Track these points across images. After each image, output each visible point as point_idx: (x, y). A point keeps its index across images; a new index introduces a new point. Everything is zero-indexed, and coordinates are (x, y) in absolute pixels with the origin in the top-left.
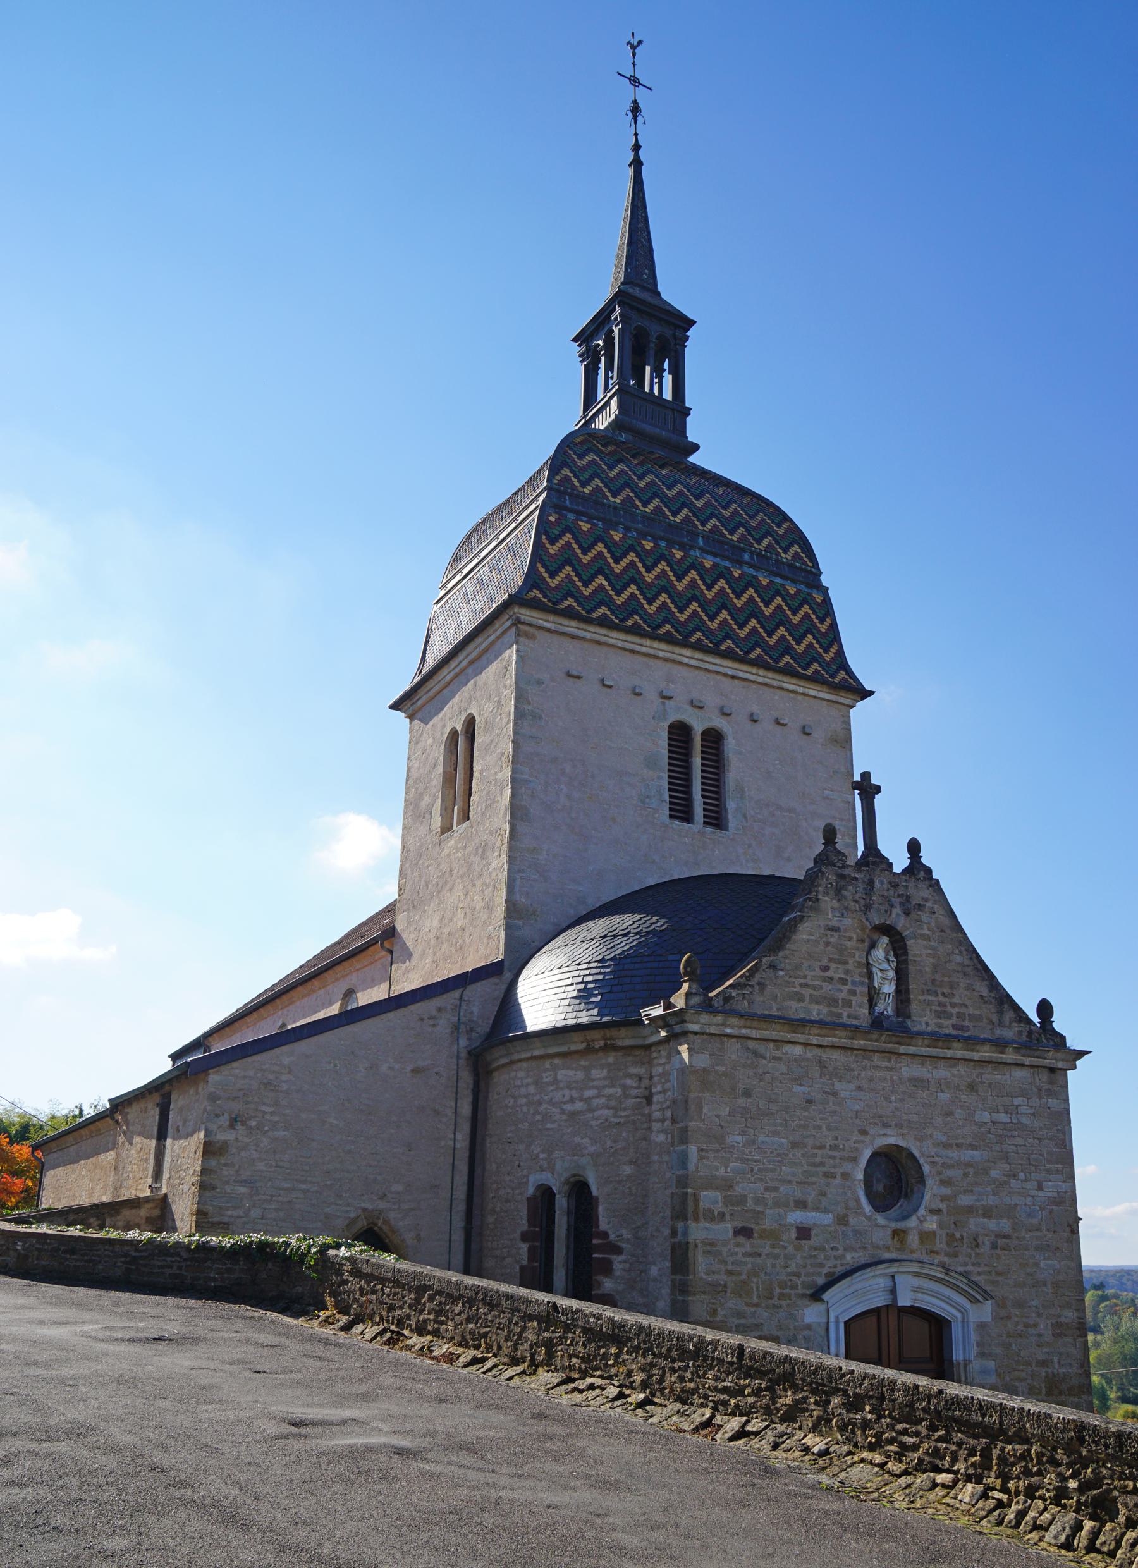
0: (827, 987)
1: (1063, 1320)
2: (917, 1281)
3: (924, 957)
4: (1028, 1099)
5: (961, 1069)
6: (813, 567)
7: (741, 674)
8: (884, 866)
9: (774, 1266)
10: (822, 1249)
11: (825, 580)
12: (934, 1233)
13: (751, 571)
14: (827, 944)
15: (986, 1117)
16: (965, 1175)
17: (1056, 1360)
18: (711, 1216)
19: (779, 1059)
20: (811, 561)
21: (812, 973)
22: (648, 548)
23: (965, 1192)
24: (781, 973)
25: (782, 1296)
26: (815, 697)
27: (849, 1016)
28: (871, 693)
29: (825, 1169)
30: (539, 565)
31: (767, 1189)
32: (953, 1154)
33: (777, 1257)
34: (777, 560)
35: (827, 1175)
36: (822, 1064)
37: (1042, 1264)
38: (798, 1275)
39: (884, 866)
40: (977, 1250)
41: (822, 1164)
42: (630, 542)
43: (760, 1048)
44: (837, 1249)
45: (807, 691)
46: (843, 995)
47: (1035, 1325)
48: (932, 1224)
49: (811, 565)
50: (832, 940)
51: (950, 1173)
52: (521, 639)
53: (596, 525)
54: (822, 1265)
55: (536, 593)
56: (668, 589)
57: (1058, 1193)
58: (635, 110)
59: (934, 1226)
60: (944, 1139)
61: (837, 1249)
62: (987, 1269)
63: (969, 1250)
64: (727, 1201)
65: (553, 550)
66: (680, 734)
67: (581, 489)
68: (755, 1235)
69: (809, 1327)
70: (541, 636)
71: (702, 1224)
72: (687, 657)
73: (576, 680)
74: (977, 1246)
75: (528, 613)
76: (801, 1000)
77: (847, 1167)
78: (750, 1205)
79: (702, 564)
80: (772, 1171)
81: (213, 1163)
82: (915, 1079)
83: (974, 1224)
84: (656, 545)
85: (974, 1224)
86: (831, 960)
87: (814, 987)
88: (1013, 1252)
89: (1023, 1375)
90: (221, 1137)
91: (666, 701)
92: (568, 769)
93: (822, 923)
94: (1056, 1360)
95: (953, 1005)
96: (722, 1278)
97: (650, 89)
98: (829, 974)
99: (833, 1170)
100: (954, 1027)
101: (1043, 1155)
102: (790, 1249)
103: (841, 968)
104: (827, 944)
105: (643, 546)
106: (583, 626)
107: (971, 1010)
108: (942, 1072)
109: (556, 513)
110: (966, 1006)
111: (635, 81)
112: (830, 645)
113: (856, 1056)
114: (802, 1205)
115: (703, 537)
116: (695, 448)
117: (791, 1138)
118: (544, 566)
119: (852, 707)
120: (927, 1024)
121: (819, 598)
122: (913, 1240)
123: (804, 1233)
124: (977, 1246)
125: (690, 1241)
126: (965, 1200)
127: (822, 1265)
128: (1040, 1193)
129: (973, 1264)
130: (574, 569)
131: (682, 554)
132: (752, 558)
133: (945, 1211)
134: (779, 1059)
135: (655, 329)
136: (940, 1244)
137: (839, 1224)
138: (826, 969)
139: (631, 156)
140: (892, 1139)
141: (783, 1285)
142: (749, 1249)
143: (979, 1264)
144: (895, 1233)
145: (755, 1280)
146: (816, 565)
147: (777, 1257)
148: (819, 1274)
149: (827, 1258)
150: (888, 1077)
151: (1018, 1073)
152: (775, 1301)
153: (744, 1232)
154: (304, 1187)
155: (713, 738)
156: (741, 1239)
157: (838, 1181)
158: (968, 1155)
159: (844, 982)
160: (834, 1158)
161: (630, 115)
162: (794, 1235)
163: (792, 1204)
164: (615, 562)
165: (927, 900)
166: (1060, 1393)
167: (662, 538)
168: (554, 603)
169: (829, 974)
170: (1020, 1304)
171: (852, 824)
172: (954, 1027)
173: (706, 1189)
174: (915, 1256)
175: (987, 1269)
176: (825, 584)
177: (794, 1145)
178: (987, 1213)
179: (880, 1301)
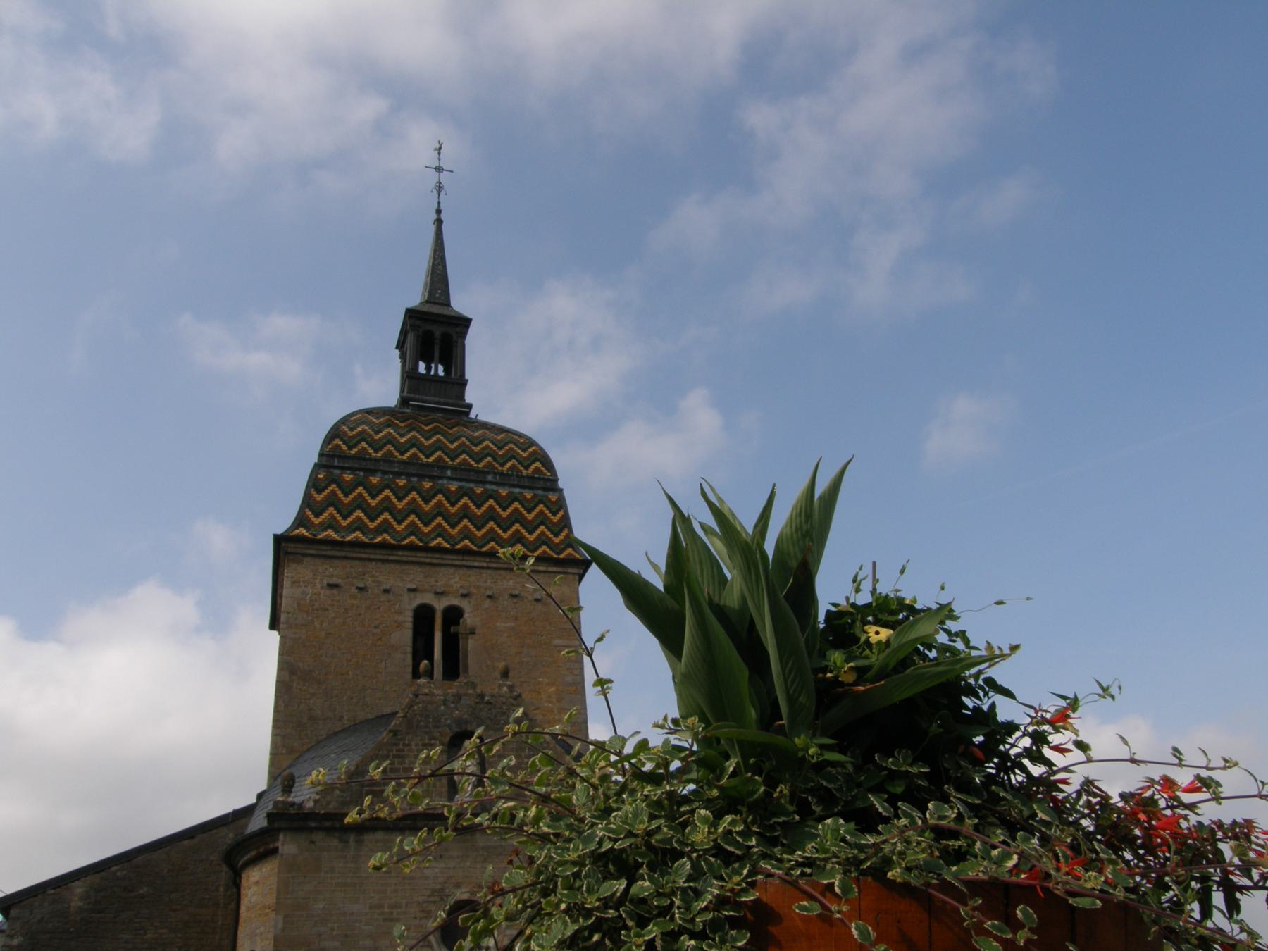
6: (551, 476)
7: (476, 564)
11: (561, 484)
20: (549, 471)
22: (529, 497)
30: (307, 510)
34: (517, 476)
42: (386, 482)
49: (549, 474)
53: (358, 475)
55: (302, 531)
56: (390, 508)
58: (439, 188)
65: (319, 498)
66: (423, 616)
67: (348, 452)
75: (293, 545)
84: (409, 481)
109: (324, 471)
112: (561, 530)
118: (310, 510)
121: (553, 497)
125: (1209, 825)
131: (431, 484)
132: (495, 478)
135: (438, 331)
139: (435, 217)
155: (453, 615)
164: (553, 515)
167: (413, 475)
168: (478, 547)
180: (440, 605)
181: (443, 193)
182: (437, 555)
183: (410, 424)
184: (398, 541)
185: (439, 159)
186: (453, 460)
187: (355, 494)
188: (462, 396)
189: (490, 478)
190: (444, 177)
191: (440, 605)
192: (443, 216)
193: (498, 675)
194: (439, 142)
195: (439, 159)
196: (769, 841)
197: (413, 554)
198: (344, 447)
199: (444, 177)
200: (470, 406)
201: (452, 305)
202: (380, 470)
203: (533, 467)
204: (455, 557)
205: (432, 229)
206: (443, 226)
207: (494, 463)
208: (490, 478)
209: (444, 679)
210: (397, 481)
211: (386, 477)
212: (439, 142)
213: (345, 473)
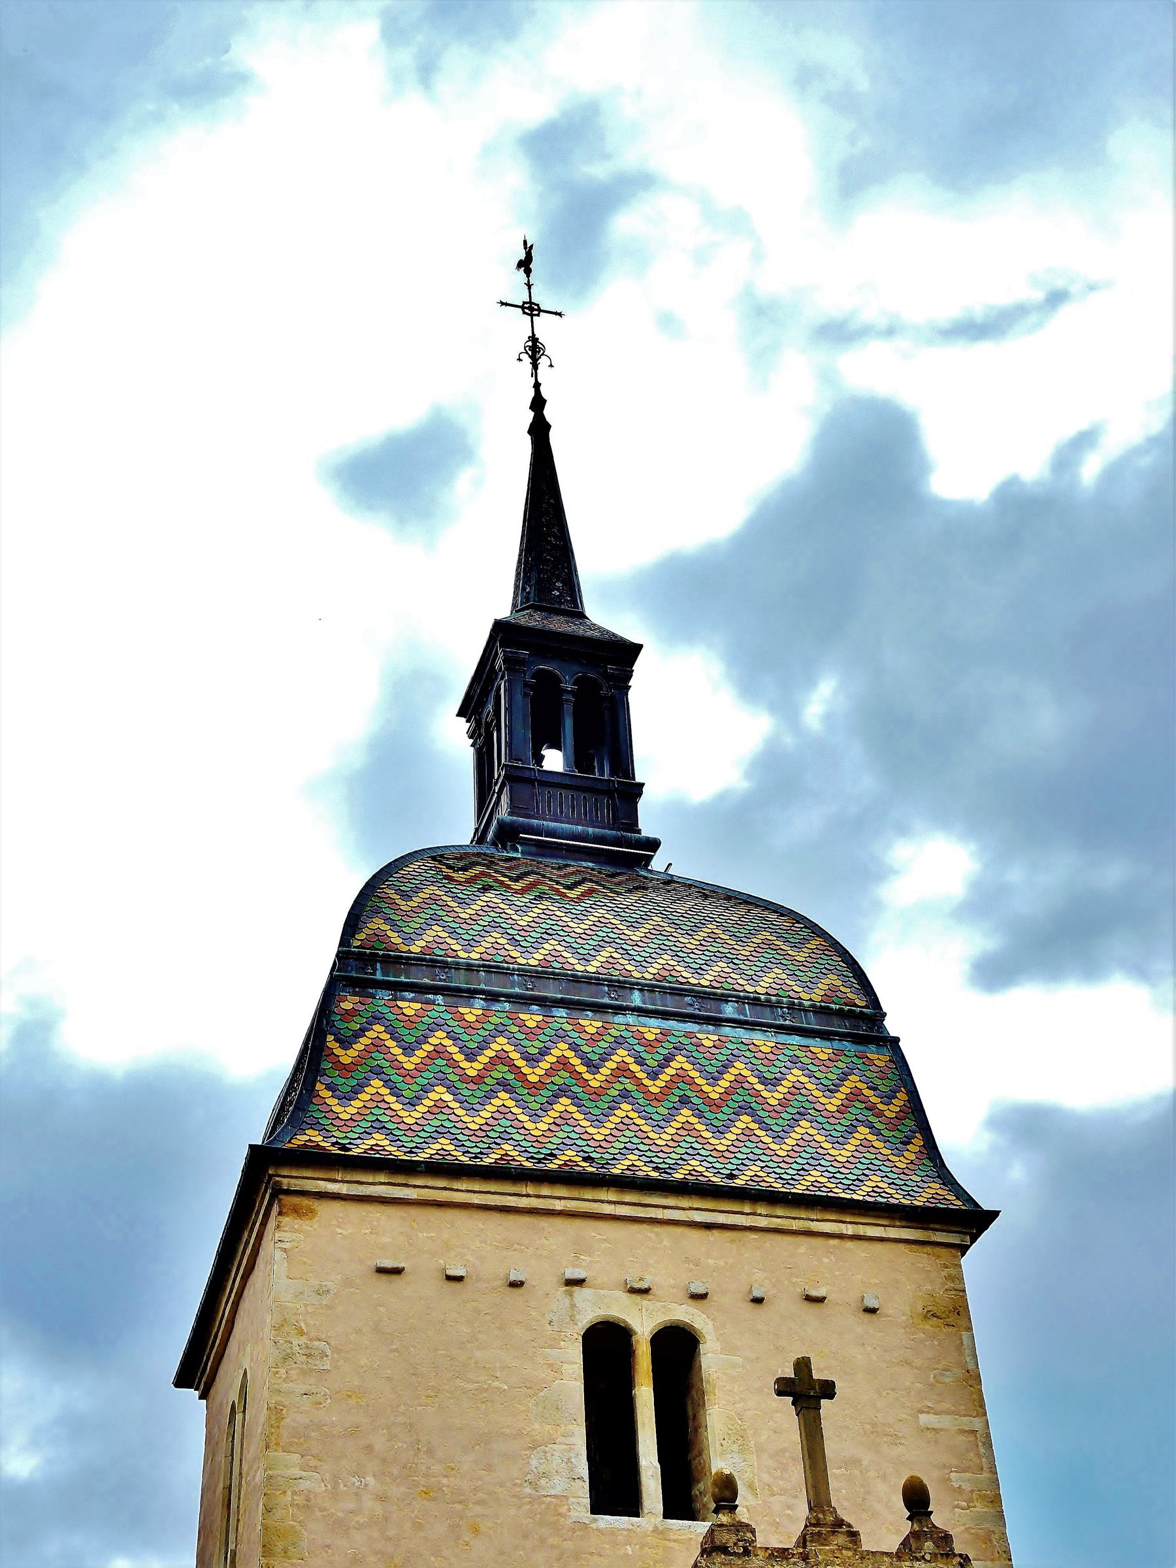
8: (841, 1539)
11: (892, 1026)
26: (881, 1240)
28: (994, 1215)
39: (841, 1539)
45: (862, 1230)
52: (286, 1220)
58: (535, 349)
70: (325, 1209)
72: (610, 1202)
73: (394, 1277)
79: (641, 1039)
91: (576, 1289)
92: (379, 1441)
97: (560, 314)
105: (522, 1025)
106: (400, 1179)
111: (531, 309)
116: (654, 845)
119: (964, 1249)
130: (387, 1083)
139: (870, 315)
146: (874, 1002)
161: (527, 360)
171: (986, 1475)
176: (893, 1033)
181: (543, 362)
182: (629, 1197)
183: (533, 885)
184: (540, 1161)
185: (529, 286)
189: (729, 1010)
190: (544, 326)
192: (548, 413)
193: (314, 1282)
194: (525, 242)
195: (529, 286)
197: (575, 1193)
199: (544, 326)
201: (588, 613)
202: (482, 992)
204: (697, 1203)
205: (525, 446)
208: (729, 1010)
210: (462, 1010)
211: (497, 1007)
212: (525, 242)
213: (403, 999)
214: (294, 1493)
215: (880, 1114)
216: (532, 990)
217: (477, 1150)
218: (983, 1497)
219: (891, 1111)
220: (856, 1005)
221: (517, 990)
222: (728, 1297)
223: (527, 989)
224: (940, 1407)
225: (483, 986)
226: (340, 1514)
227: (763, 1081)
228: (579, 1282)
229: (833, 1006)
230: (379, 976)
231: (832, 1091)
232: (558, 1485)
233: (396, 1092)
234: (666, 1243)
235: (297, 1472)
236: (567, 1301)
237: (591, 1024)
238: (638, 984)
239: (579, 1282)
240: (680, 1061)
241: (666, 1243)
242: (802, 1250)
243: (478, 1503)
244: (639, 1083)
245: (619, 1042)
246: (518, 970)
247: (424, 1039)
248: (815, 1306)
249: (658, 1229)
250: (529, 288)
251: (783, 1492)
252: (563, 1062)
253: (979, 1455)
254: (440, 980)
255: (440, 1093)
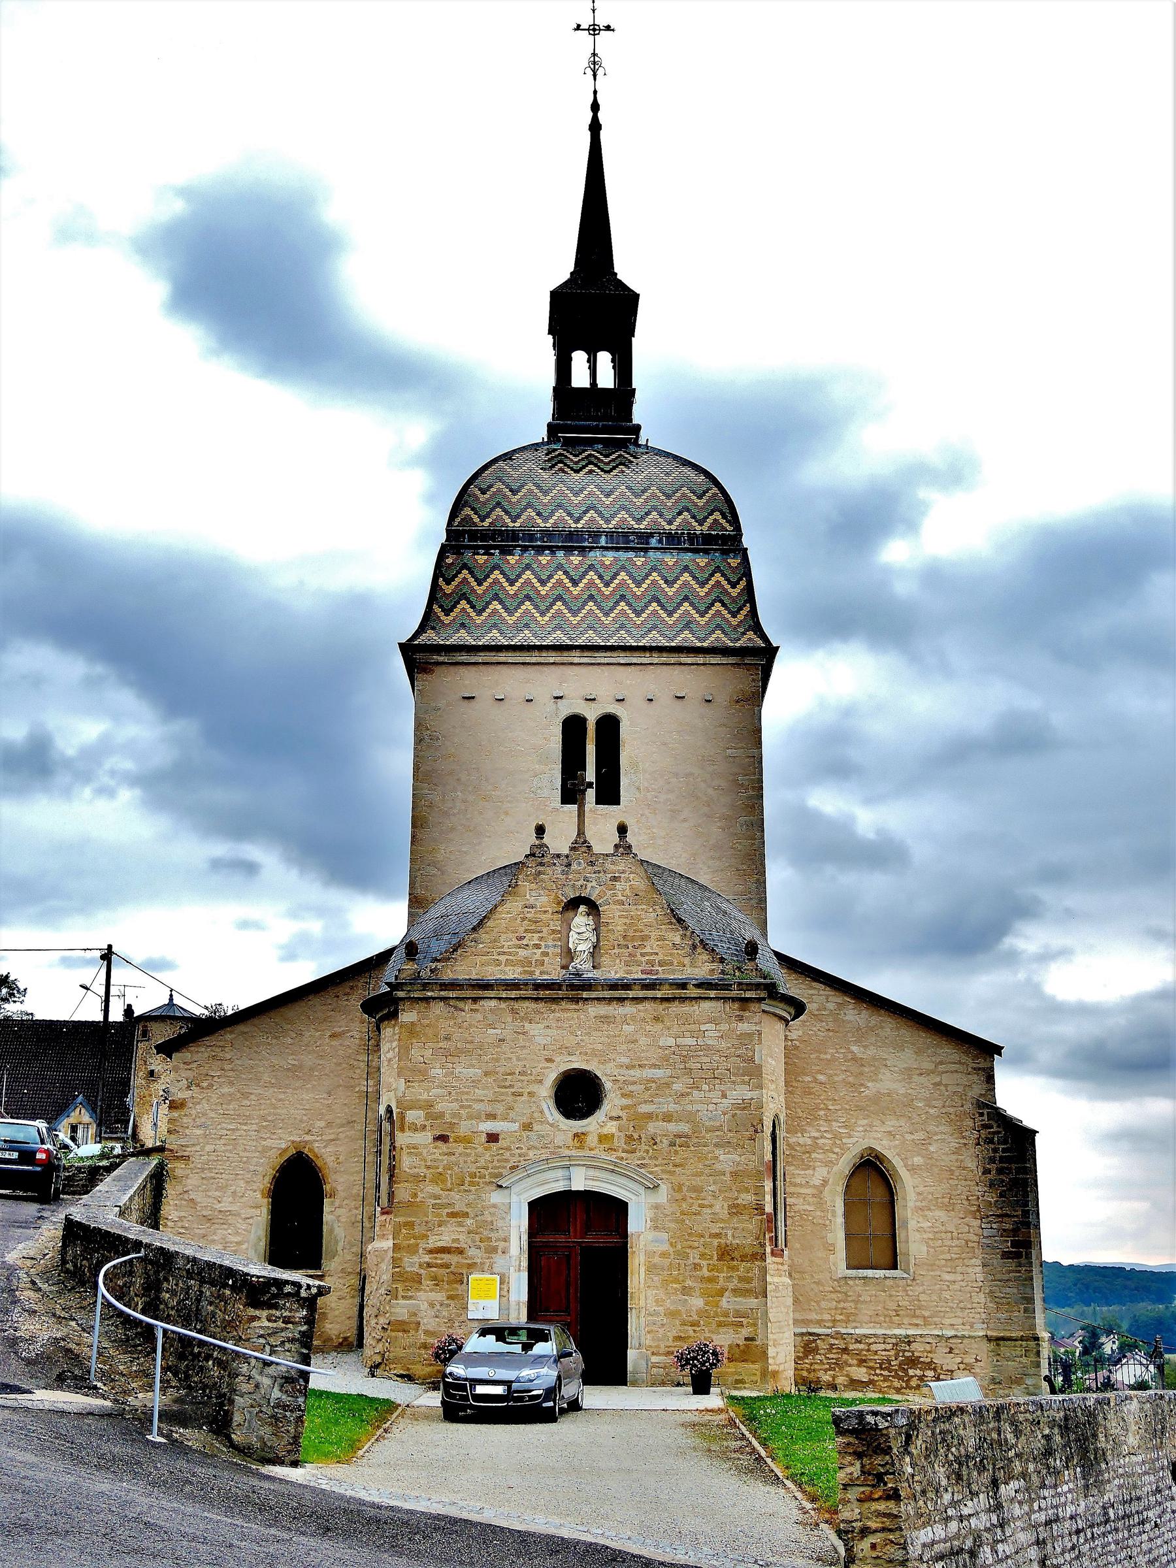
0: (522, 953)
1: (739, 1201)
2: (591, 1172)
3: (617, 918)
4: (716, 1024)
5: (648, 1005)
7: (635, 660)
8: (584, 849)
9: (465, 1162)
10: (508, 1149)
12: (613, 1135)
13: (659, 554)
14: (523, 919)
15: (671, 1042)
16: (647, 1089)
17: (730, 1233)
18: (415, 1128)
19: (477, 1010)
21: (509, 943)
23: (645, 1102)
24: (481, 946)
25: (472, 1184)
27: (541, 973)
29: (513, 1090)
31: (461, 1107)
32: (636, 1073)
33: (468, 1155)
35: (513, 1094)
36: (514, 1011)
37: (722, 1158)
38: (486, 1168)
39: (584, 849)
40: (655, 1147)
41: (511, 1086)
43: (461, 1004)
44: (522, 1148)
46: (538, 957)
47: (711, 1206)
48: (611, 1128)
50: (528, 915)
51: (631, 1088)
54: (507, 1161)
57: (743, 1100)
58: (594, 65)
59: (614, 1130)
60: (626, 1061)
61: (522, 1148)
62: (666, 1162)
63: (647, 1147)
64: (428, 1116)
66: (573, 727)
68: (451, 1140)
69: (494, 1206)
71: (408, 1133)
74: (655, 1144)
76: (498, 963)
77: (534, 1088)
78: (447, 1118)
79: (603, 564)
80: (467, 1093)
81: (175, 1114)
82: (601, 1017)
83: (652, 1127)
85: (652, 1127)
86: (526, 931)
87: (510, 954)
88: (692, 1148)
89: (696, 1244)
90: (181, 1095)
93: (520, 904)
94: (730, 1233)
95: (642, 955)
96: (422, 1171)
98: (525, 942)
99: (521, 1090)
100: (643, 972)
101: (729, 1070)
102: (480, 1149)
103: (536, 935)
104: (523, 919)
107: (661, 957)
108: (629, 1009)
110: (657, 954)
113: (545, 1003)
114: (492, 1116)
115: (606, 536)
117: (484, 1069)
120: (616, 973)
122: (592, 1140)
123: (493, 1138)
124: (655, 1144)
126: (645, 1108)
127: (507, 1161)
128: (724, 1100)
129: (650, 1158)
133: (625, 1119)
134: (477, 1010)
136: (619, 1142)
137: (524, 1130)
138: (521, 938)
140: (578, 1064)
141: (472, 1175)
142: (445, 1150)
143: (656, 1158)
144: (576, 1135)
145: (449, 1172)
147: (468, 1155)
148: (505, 1167)
149: (513, 1155)
150: (575, 1016)
151: (706, 1005)
152: (466, 1187)
153: (443, 1138)
154: (245, 1128)
155: (609, 726)
156: (440, 1144)
157: (525, 1098)
158: (649, 1073)
159: (537, 946)
160: (523, 1081)
161: (590, 72)
162: (484, 1138)
163: (483, 1117)
165: (624, 872)
166: (733, 1259)
169: (525, 942)
170: (697, 1190)
172: (643, 972)
173: (410, 1109)
174: (592, 1153)
175: (666, 1162)
177: (486, 1074)
178: (668, 1118)
179: (559, 1187)
180: (592, 715)
181: (600, 72)
186: (608, 521)
187: (490, 580)
188: (628, 415)
191: (592, 715)
196: (691, 966)
198: (476, 519)
200: (638, 428)
203: (710, 520)
205: (587, 136)
206: (602, 133)
207: (660, 520)
209: (597, 803)
214: (425, 801)
215: (729, 594)
216: (547, 542)
217: (511, 635)
218: (753, 788)
219: (734, 592)
220: (727, 530)
221: (539, 543)
222: (636, 699)
223: (544, 542)
224: (738, 746)
225: (520, 543)
226: (446, 809)
227: (666, 582)
228: (561, 697)
229: (713, 532)
230: (466, 542)
231: (702, 584)
232: (546, 793)
233: (473, 607)
234: (606, 674)
235: (427, 791)
236: (554, 706)
237: (576, 559)
238: (604, 532)
239: (561, 697)
240: (623, 575)
241: (606, 674)
242: (676, 672)
243: (508, 802)
244: (599, 590)
245: (591, 567)
246: (540, 531)
247: (487, 576)
248: (680, 700)
249: (603, 668)
250: (594, 12)
251: (654, 790)
252: (560, 582)
253: (755, 768)
254: (499, 541)
255: (496, 605)
